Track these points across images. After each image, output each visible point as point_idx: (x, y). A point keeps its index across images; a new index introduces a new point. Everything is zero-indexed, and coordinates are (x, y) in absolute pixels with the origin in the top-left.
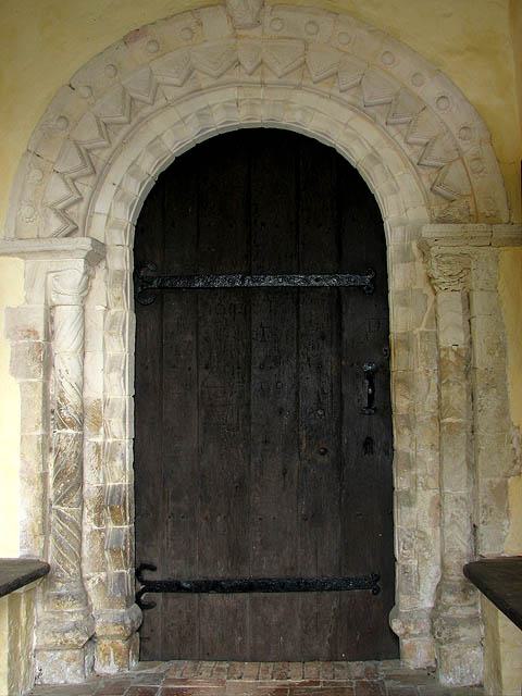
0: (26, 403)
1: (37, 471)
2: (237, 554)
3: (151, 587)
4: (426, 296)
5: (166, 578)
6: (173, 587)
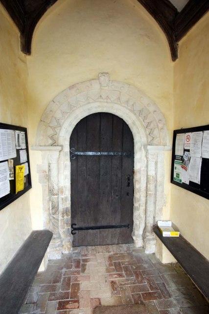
0: (44, 191)
1: (47, 207)
2: (96, 220)
3: (75, 229)
4: (145, 161)
5: (78, 227)
6: (80, 229)
